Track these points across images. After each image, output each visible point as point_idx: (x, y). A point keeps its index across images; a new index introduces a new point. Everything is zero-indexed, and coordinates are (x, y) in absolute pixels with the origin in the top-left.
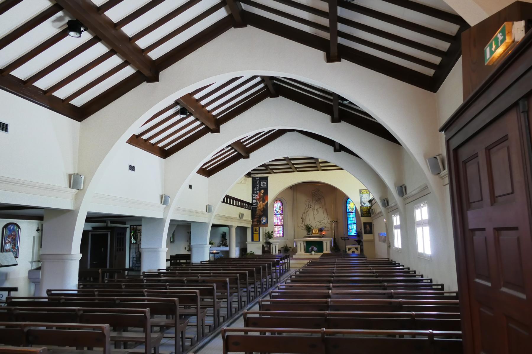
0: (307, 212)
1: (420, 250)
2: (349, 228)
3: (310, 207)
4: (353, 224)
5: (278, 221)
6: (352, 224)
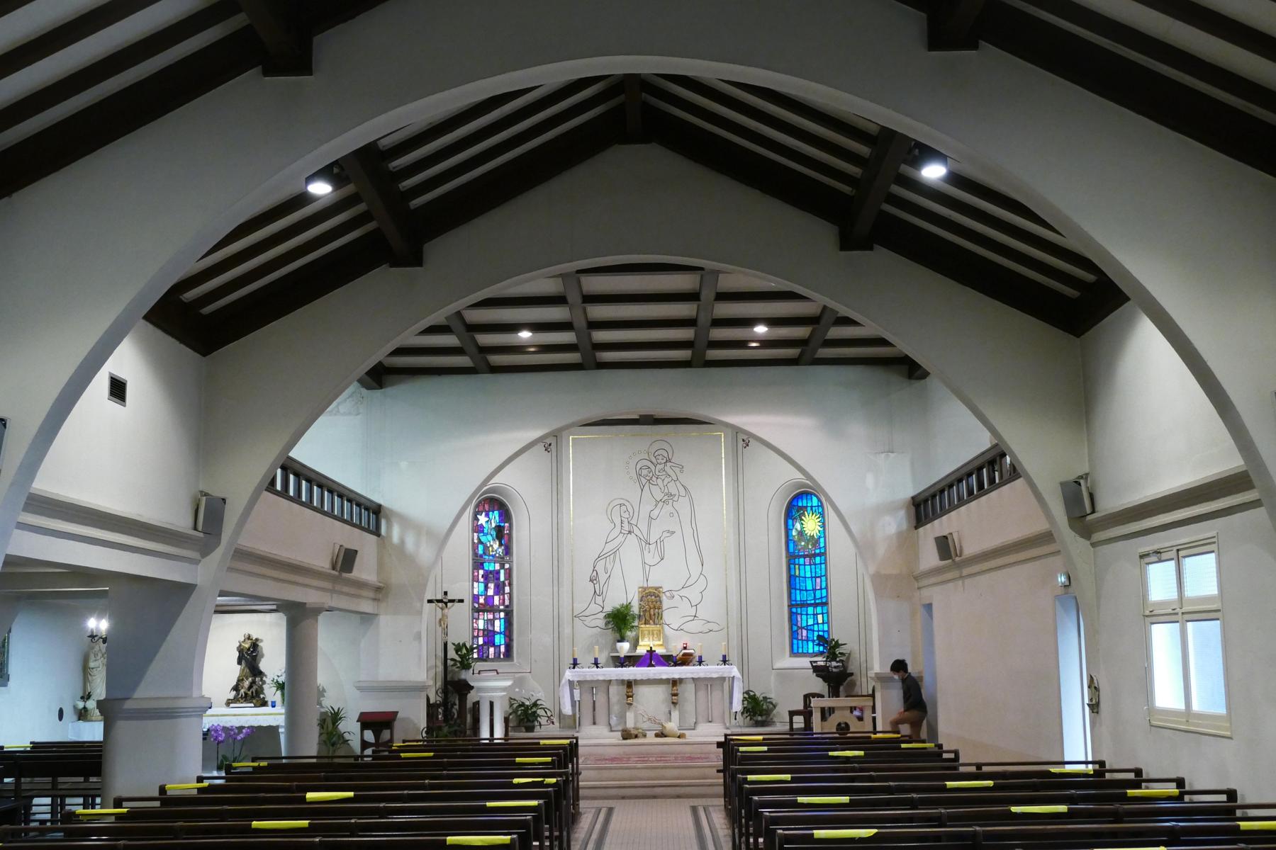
0: (615, 552)
2: (794, 622)
3: (630, 532)
4: (815, 605)
5: (491, 592)
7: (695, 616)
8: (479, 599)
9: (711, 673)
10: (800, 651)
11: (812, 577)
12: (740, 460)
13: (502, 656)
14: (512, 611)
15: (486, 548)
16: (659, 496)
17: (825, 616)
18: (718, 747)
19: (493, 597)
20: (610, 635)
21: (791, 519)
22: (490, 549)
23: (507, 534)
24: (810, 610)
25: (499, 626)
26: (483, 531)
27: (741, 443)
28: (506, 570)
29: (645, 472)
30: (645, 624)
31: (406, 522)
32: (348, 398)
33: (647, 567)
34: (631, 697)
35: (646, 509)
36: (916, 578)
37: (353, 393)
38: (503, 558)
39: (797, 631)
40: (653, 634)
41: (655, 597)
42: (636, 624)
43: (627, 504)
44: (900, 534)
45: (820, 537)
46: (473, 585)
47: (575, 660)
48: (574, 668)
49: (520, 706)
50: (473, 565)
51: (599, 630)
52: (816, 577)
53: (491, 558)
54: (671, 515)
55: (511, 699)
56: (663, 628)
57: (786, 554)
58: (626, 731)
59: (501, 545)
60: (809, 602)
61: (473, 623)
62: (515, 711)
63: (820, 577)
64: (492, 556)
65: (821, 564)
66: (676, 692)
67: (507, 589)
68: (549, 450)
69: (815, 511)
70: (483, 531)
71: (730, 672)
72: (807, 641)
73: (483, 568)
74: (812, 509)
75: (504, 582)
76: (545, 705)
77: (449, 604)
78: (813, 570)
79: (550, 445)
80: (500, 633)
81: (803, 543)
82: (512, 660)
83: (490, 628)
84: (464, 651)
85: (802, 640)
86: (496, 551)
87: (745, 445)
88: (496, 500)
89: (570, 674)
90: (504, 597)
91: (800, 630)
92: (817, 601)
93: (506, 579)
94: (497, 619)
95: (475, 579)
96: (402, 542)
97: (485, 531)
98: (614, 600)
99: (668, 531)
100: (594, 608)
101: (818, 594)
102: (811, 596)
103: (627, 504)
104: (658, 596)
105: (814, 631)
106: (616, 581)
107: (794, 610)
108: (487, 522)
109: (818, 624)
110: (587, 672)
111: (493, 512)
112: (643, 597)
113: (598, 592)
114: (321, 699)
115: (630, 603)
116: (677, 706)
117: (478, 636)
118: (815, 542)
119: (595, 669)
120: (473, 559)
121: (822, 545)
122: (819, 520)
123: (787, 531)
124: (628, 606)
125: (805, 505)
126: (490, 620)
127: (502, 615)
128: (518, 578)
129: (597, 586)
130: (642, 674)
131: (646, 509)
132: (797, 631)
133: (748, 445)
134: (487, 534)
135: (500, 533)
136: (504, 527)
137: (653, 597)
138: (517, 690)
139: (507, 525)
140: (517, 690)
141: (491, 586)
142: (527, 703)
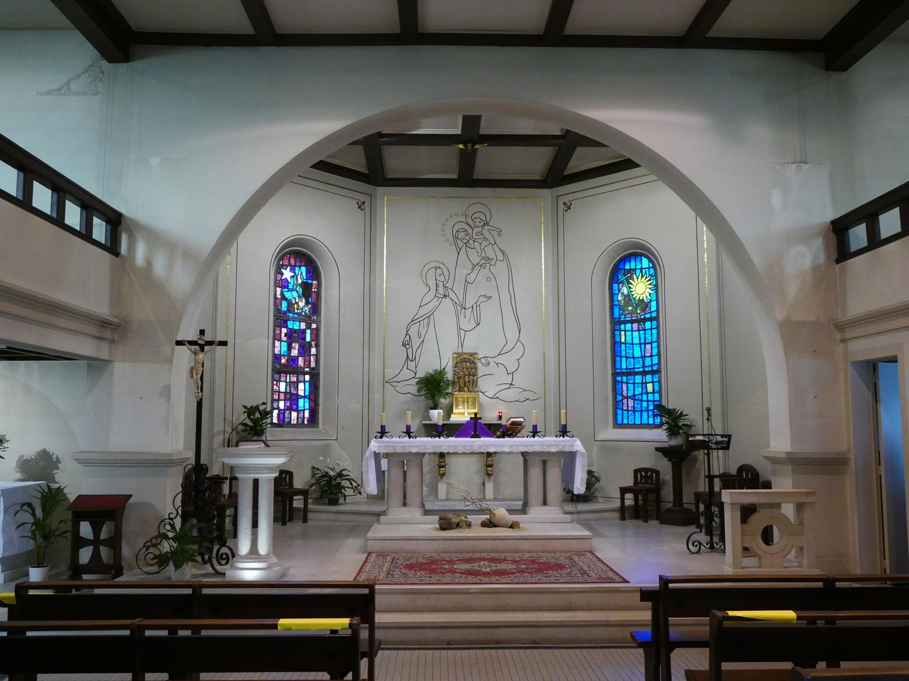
1: (626, 495)
2: (619, 391)
3: (445, 296)
4: (644, 373)
5: (295, 353)
6: (638, 373)
7: (511, 384)
8: (281, 359)
9: (549, 446)
10: (625, 421)
11: (640, 344)
12: (560, 222)
13: (306, 422)
14: (319, 373)
15: (290, 304)
16: (476, 259)
17: (656, 385)
18: (642, 599)
19: (297, 358)
20: (423, 401)
21: (616, 283)
22: (295, 306)
23: (315, 292)
24: (638, 379)
25: (303, 389)
26: (288, 286)
27: (561, 206)
28: (312, 330)
29: (461, 235)
30: (459, 391)
31: (155, 238)
32: (83, 73)
33: (462, 333)
34: (444, 467)
35: (462, 271)
36: (840, 327)
37: (90, 66)
38: (310, 317)
39: (622, 400)
40: (468, 402)
41: (471, 363)
42: (450, 391)
43: (442, 266)
44: (816, 269)
45: (651, 301)
46: (274, 343)
47: (383, 427)
48: (381, 437)
49: (323, 476)
50: (274, 322)
51: (411, 396)
52: (645, 344)
53: (296, 316)
54: (488, 279)
55: (314, 468)
56: (477, 394)
57: (611, 321)
58: (445, 519)
59: (307, 303)
60: (636, 370)
61: (273, 385)
62: (318, 482)
63: (651, 343)
64: (297, 314)
65: (652, 329)
66: (491, 463)
67: (313, 351)
68: (362, 208)
69: (646, 273)
70: (287, 287)
71: (572, 446)
72: (634, 411)
73: (286, 327)
74: (641, 271)
75: (310, 343)
76: (352, 476)
77: (207, 348)
78: (643, 336)
79: (364, 203)
80: (305, 397)
81: (630, 308)
82: (317, 426)
83: (293, 392)
84: (257, 415)
85: (628, 410)
86: (302, 309)
87: (566, 209)
88: (305, 255)
89: (376, 445)
90: (310, 358)
91: (625, 400)
92: (647, 369)
93: (312, 340)
94: (301, 382)
95: (277, 337)
96: (149, 263)
97: (290, 287)
98: (427, 365)
99: (485, 296)
100: (410, 374)
101: (648, 361)
102: (639, 363)
103: (442, 266)
104: (474, 362)
105: (642, 401)
106: (430, 346)
107: (619, 379)
108: (292, 277)
109: (647, 393)
110: (398, 443)
111: (300, 267)
112: (457, 363)
113: (410, 357)
114: (55, 471)
115: (444, 369)
116: (492, 477)
117: (278, 400)
118: (644, 305)
119: (407, 439)
120: (275, 316)
121: (654, 308)
122: (649, 282)
123: (612, 295)
124: (442, 373)
125: (633, 267)
126: (294, 382)
127: (307, 378)
128: (325, 340)
129: (410, 351)
130: (464, 446)
131: (462, 271)
132: (622, 400)
133: (570, 209)
134: (292, 290)
135: (309, 292)
136: (311, 284)
137: (468, 364)
138: (321, 458)
139: (315, 282)
140: (321, 458)
141: (296, 346)
142: (332, 473)
